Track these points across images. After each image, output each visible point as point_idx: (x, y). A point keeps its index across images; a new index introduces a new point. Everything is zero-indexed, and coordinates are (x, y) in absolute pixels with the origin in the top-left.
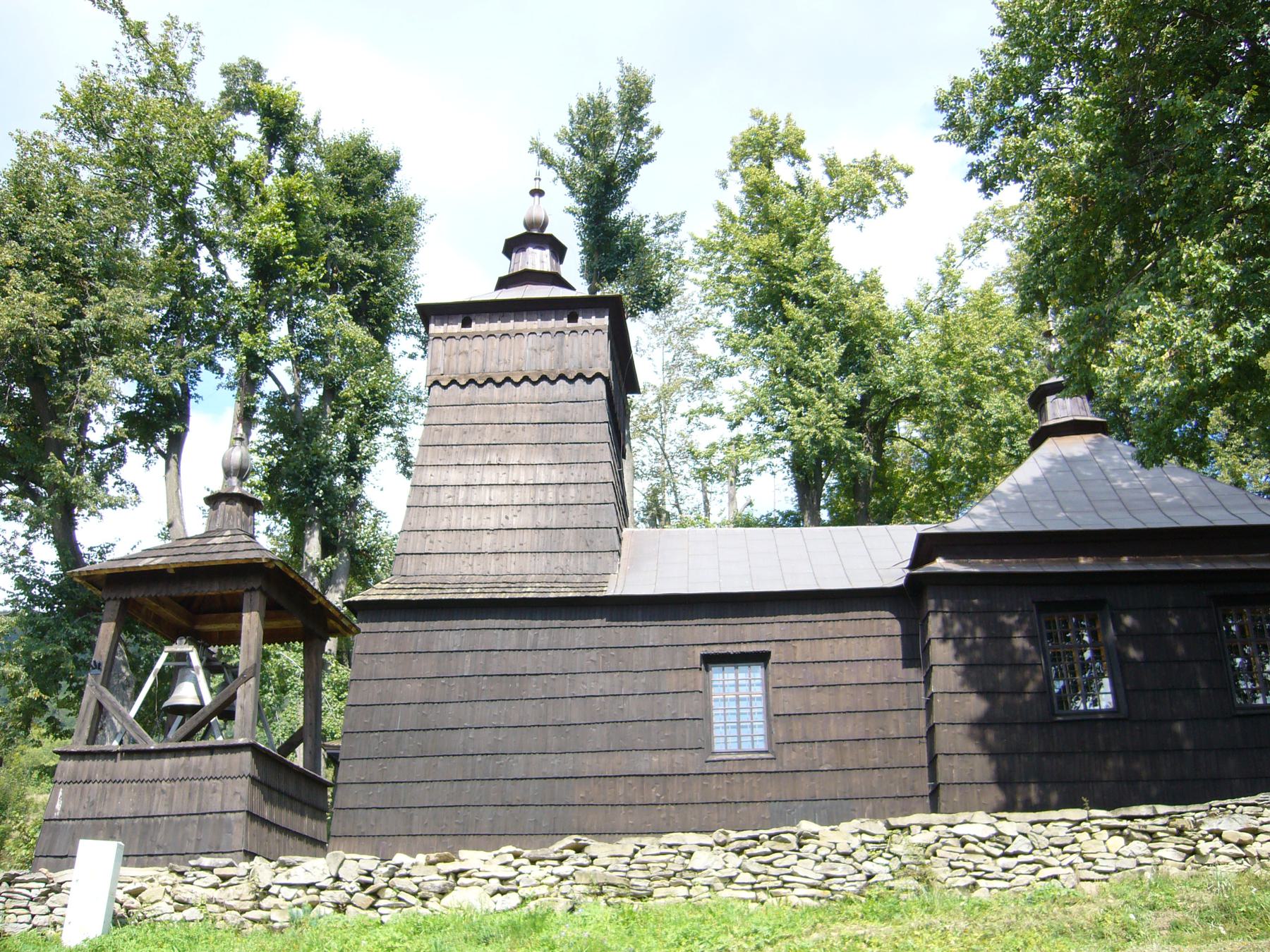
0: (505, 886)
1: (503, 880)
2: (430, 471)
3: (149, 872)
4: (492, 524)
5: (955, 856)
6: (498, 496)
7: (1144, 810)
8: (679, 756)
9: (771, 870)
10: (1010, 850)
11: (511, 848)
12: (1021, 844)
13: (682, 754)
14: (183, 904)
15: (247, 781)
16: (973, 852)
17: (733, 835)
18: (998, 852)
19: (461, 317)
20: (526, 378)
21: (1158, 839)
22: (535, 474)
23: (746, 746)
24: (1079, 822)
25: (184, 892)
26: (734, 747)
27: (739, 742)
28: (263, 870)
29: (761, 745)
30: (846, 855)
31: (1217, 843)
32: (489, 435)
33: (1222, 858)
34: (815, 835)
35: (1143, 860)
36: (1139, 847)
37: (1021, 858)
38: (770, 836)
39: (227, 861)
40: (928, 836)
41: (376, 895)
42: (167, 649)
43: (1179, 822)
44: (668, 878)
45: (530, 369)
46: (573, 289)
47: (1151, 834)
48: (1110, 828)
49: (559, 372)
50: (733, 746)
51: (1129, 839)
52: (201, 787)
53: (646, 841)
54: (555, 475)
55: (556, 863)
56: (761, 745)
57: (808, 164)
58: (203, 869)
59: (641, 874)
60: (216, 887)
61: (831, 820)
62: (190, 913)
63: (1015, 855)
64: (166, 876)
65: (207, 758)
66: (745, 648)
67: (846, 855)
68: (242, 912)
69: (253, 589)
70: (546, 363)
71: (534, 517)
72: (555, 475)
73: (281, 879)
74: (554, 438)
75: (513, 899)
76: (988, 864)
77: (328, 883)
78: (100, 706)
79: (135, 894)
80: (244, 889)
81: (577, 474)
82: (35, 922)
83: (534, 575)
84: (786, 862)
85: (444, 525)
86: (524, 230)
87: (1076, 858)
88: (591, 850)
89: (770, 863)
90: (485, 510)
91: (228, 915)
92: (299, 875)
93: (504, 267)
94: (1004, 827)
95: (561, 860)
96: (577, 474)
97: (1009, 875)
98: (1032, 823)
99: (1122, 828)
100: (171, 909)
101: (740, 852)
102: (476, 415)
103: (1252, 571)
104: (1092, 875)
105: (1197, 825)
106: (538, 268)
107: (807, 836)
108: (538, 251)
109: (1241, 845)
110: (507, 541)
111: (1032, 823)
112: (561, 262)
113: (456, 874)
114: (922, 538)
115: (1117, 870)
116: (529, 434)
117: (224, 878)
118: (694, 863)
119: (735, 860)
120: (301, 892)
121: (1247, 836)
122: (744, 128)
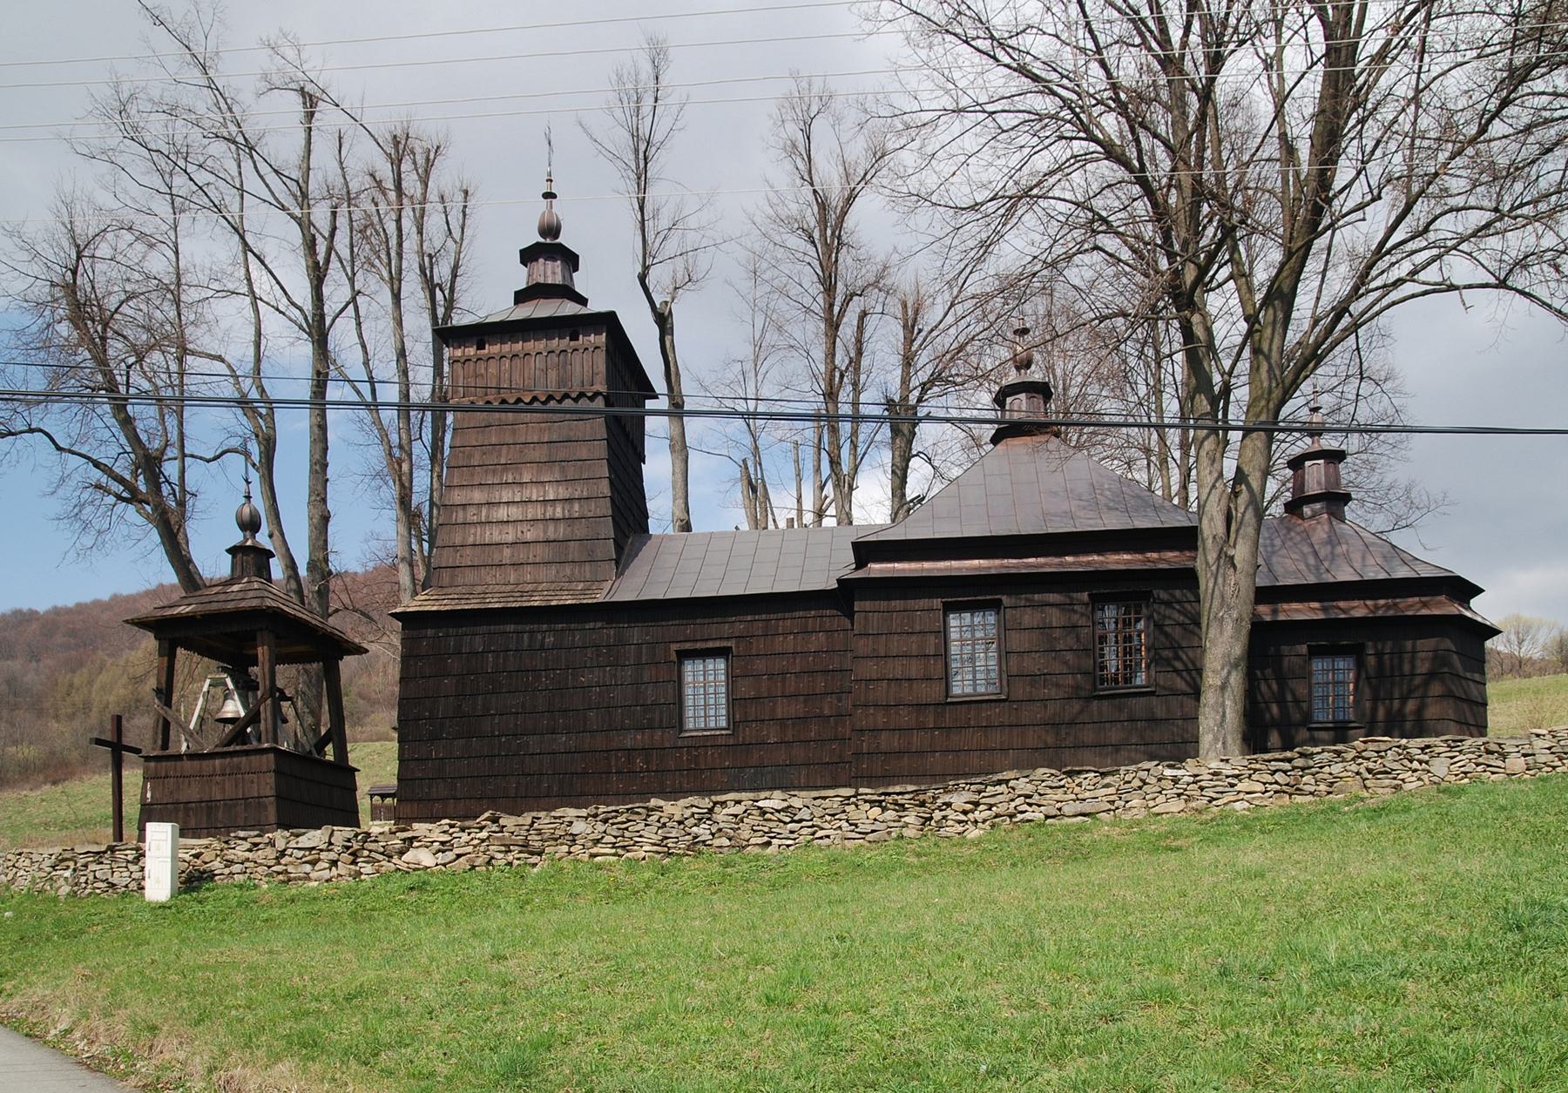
0: (445, 846)
1: (443, 843)
2: (457, 492)
3: (205, 841)
4: (510, 538)
6: (515, 512)
12: (805, 814)
17: (602, 808)
19: (475, 340)
21: (905, 809)
24: (848, 798)
25: (230, 854)
27: (975, 685)
28: (280, 837)
29: (723, 724)
30: (680, 823)
36: (890, 815)
40: (739, 809)
41: (354, 854)
43: (921, 797)
46: (583, 301)
50: (969, 690)
51: (884, 809)
53: (542, 814)
54: (563, 492)
60: (250, 850)
62: (237, 868)
65: (244, 759)
66: (710, 645)
71: (545, 532)
75: (450, 855)
77: (324, 847)
79: (197, 856)
80: (270, 853)
81: (579, 491)
85: (471, 540)
87: (844, 824)
88: (502, 822)
93: (520, 278)
94: (797, 803)
95: (481, 829)
96: (579, 491)
101: (605, 821)
104: (853, 835)
110: (522, 555)
112: (576, 269)
113: (412, 839)
117: (256, 845)
118: (575, 829)
119: (600, 827)
121: (969, 806)
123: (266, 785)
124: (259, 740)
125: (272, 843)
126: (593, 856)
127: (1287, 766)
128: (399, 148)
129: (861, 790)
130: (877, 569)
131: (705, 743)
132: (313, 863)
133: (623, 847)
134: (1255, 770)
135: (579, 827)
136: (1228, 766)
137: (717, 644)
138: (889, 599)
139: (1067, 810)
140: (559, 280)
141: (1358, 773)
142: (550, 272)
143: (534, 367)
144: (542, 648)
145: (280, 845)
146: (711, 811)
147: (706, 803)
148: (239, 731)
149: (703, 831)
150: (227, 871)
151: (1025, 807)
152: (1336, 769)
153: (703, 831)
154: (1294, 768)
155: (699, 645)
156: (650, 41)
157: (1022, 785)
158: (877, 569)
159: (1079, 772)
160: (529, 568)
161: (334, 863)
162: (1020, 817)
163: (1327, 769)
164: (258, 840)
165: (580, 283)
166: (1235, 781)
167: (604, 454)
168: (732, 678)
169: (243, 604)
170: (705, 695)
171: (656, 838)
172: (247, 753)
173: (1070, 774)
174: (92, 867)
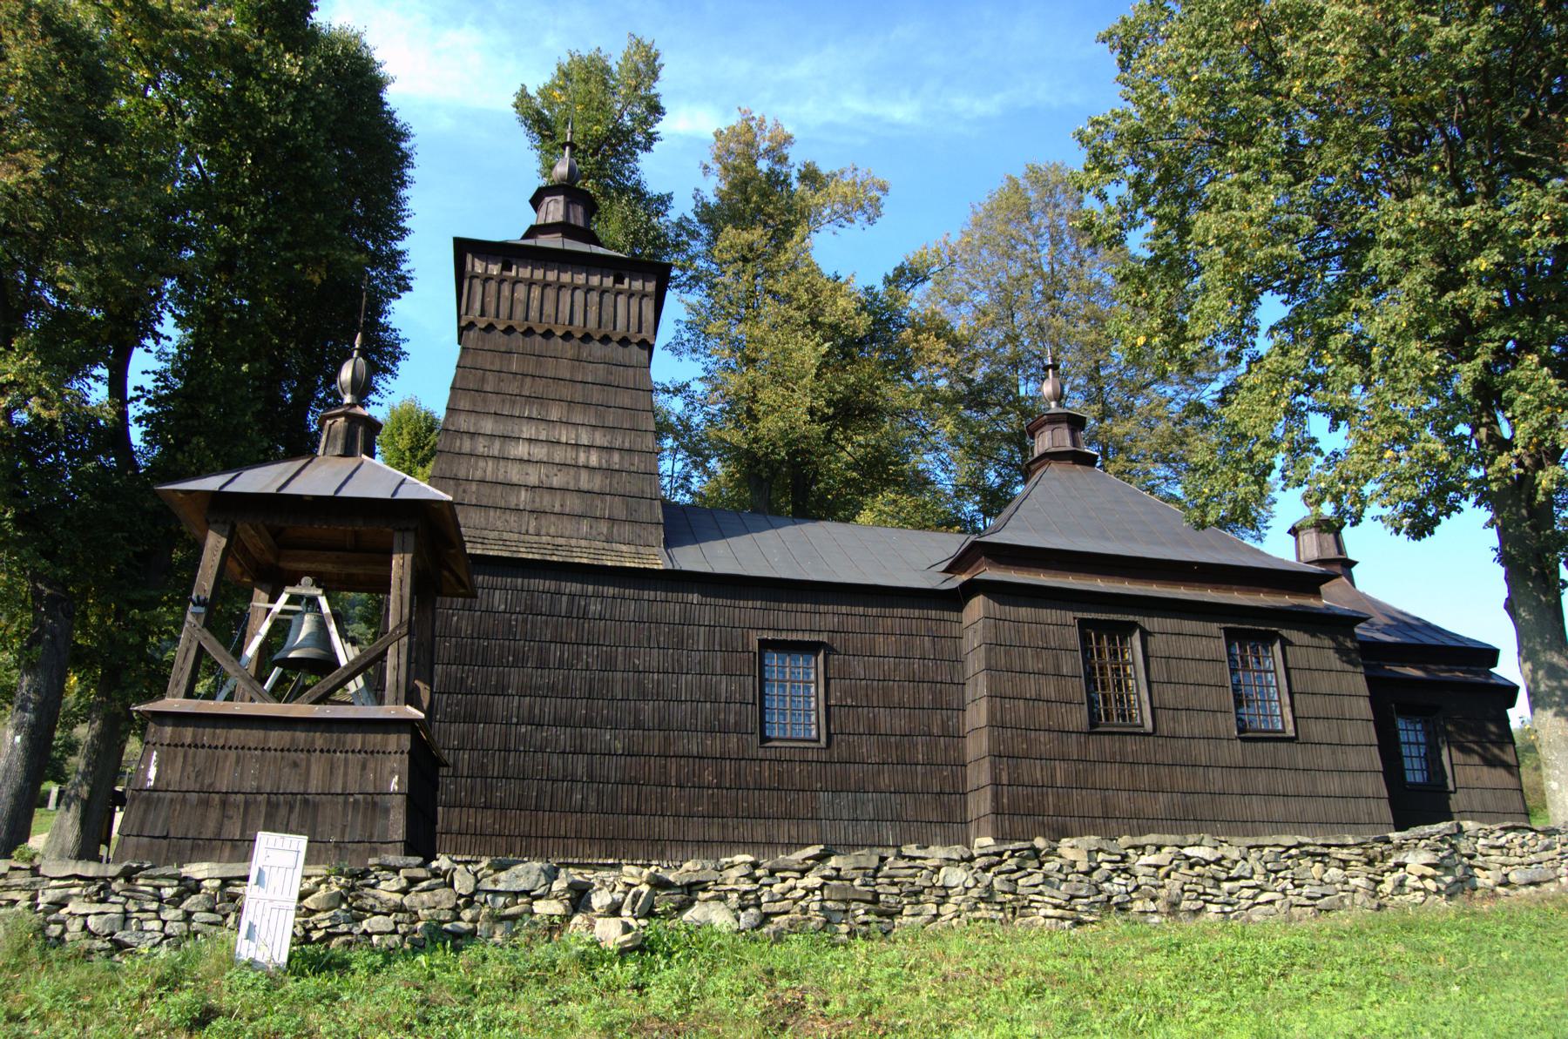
4: (533, 479)
5: (1187, 879)
10: (1233, 873)
11: (750, 858)
22: (577, 436)
36: (1334, 873)
42: (289, 589)
48: (1313, 855)
52: (346, 760)
54: (600, 439)
55: (797, 875)
69: (407, 529)
72: (600, 439)
78: (200, 649)
82: (168, 930)
85: (479, 475)
90: (525, 466)
93: (531, 218)
110: (546, 501)
124: (376, 691)
138: (1231, 590)
160: (553, 518)
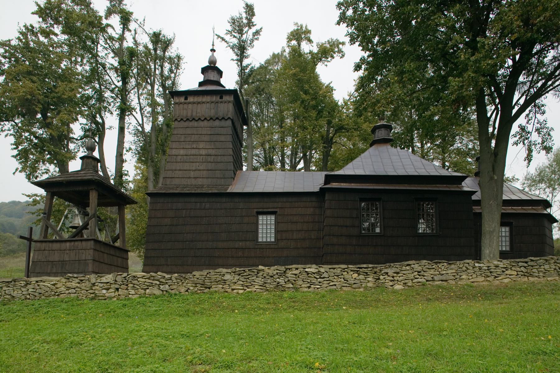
2: (174, 150)
7: (365, 266)
8: (248, 243)
9: (248, 281)
12: (325, 275)
13: (249, 242)
14: (69, 288)
15: (92, 250)
16: (310, 277)
17: (238, 269)
18: (318, 277)
20: (205, 119)
23: (269, 240)
25: (69, 284)
26: (265, 240)
28: (93, 278)
29: (273, 240)
30: (271, 277)
31: (386, 276)
32: (194, 138)
33: (387, 281)
34: (263, 270)
35: (362, 281)
37: (325, 279)
38: (249, 270)
39: (82, 275)
40: (297, 272)
43: (375, 270)
44: (217, 282)
45: (207, 116)
47: (366, 273)
49: (216, 116)
51: (359, 274)
56: (273, 240)
57: (312, 44)
58: (75, 278)
59: (208, 281)
60: (79, 283)
61: (269, 265)
63: (324, 278)
64: (64, 280)
66: (269, 210)
67: (271, 277)
68: (87, 291)
70: (212, 113)
73: (98, 281)
74: (214, 140)
76: (314, 281)
79: (54, 285)
83: (205, 184)
84: (253, 278)
85: (178, 168)
86: (207, 64)
89: (248, 278)
91: (82, 292)
92: (104, 280)
93: (201, 78)
94: (322, 270)
97: (321, 284)
98: (330, 269)
99: (358, 271)
100: (65, 289)
102: (189, 131)
103: (457, 191)
105: (381, 271)
106: (212, 79)
107: (260, 271)
108: (213, 73)
109: (393, 277)
110: (197, 174)
111: (330, 269)
112: (221, 77)
114: (326, 176)
115: (354, 284)
116: (206, 138)
117: (82, 280)
118: (225, 278)
119: (237, 277)
120: (105, 285)
122: (292, 30)
123: (88, 255)
125: (89, 280)
126: (233, 290)
127: (526, 265)
128: (156, 38)
129: (350, 266)
130: (334, 185)
131: (268, 245)
132: (107, 289)
133: (247, 286)
134: (513, 266)
135: (227, 277)
136: (502, 264)
137: (272, 210)
139: (435, 278)
140: (215, 79)
141: (555, 269)
142: (212, 76)
143: (205, 108)
144: (204, 209)
145: (93, 281)
146: (285, 272)
147: (283, 268)
148: (79, 231)
149: (281, 281)
150: (67, 292)
151: (418, 276)
152: (547, 267)
153: (281, 281)
154: (529, 266)
155: (265, 210)
156: (247, 5)
157: (417, 267)
158: (334, 185)
159: (440, 263)
161: (117, 289)
162: (416, 280)
163: (542, 267)
164: (83, 278)
165: (222, 81)
166: (504, 270)
167: (231, 140)
168: (277, 223)
169: (85, 178)
170: (266, 229)
171: (261, 283)
172: (81, 240)
173: (436, 263)
174: (5, 288)
